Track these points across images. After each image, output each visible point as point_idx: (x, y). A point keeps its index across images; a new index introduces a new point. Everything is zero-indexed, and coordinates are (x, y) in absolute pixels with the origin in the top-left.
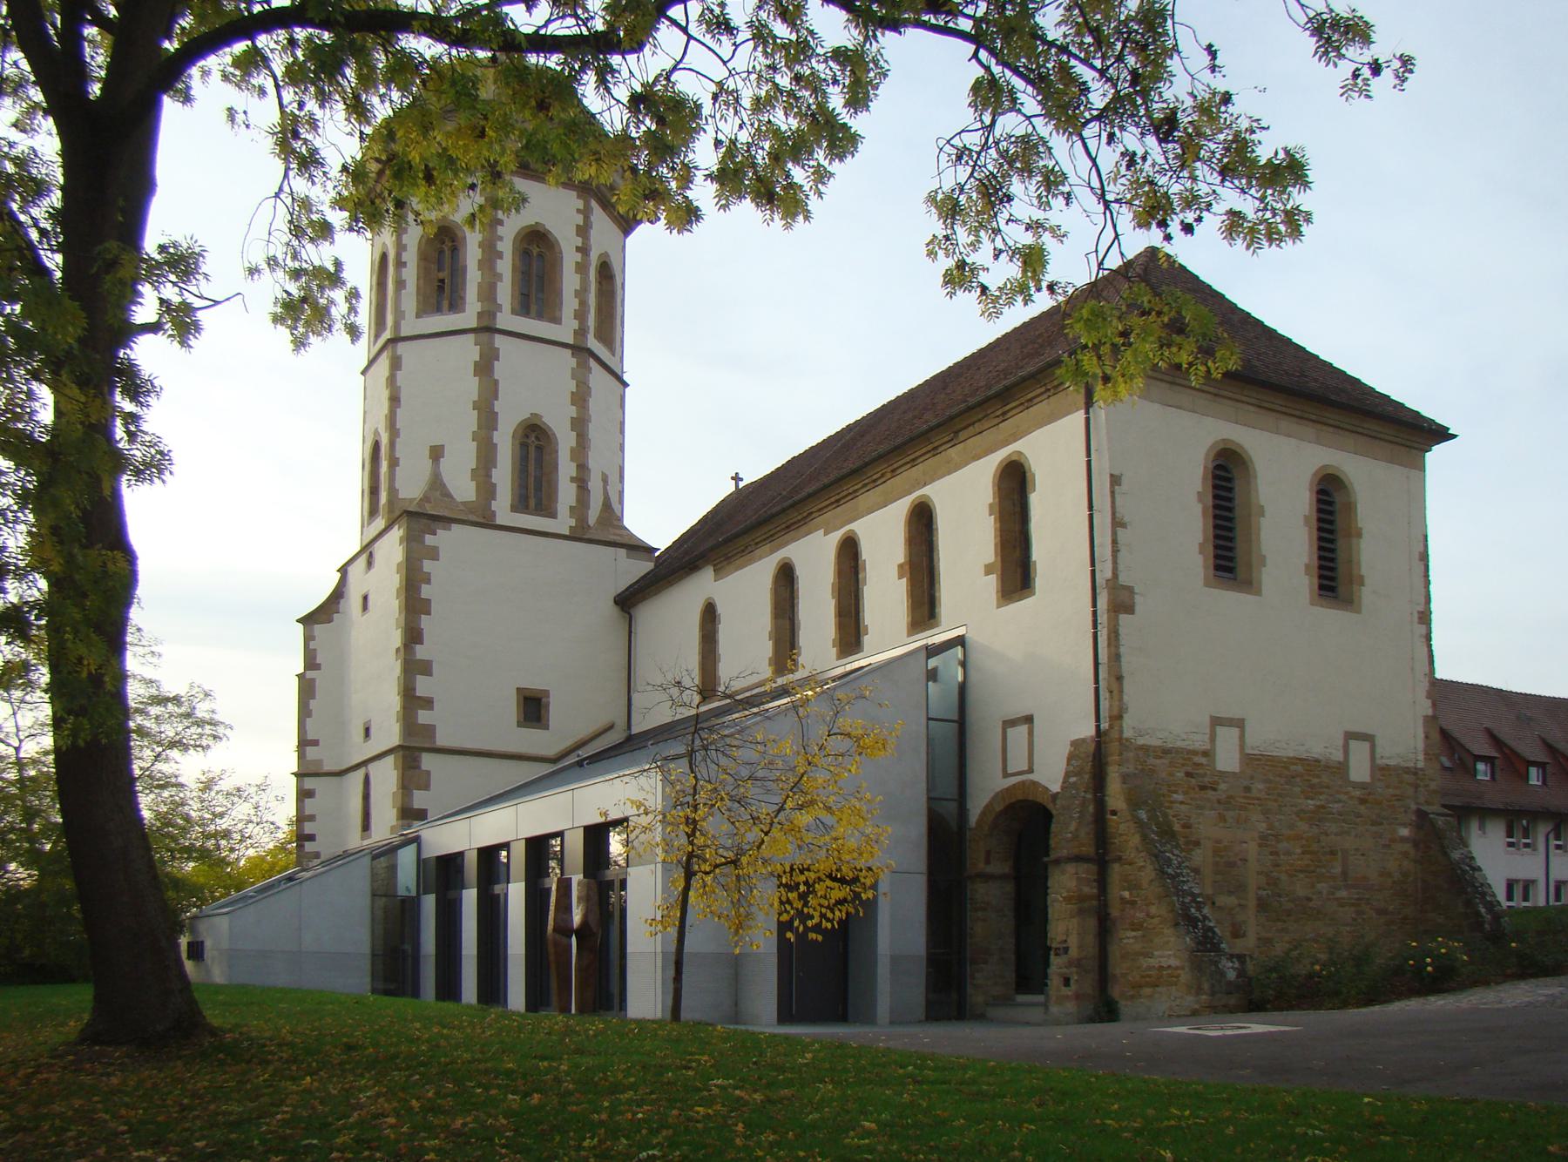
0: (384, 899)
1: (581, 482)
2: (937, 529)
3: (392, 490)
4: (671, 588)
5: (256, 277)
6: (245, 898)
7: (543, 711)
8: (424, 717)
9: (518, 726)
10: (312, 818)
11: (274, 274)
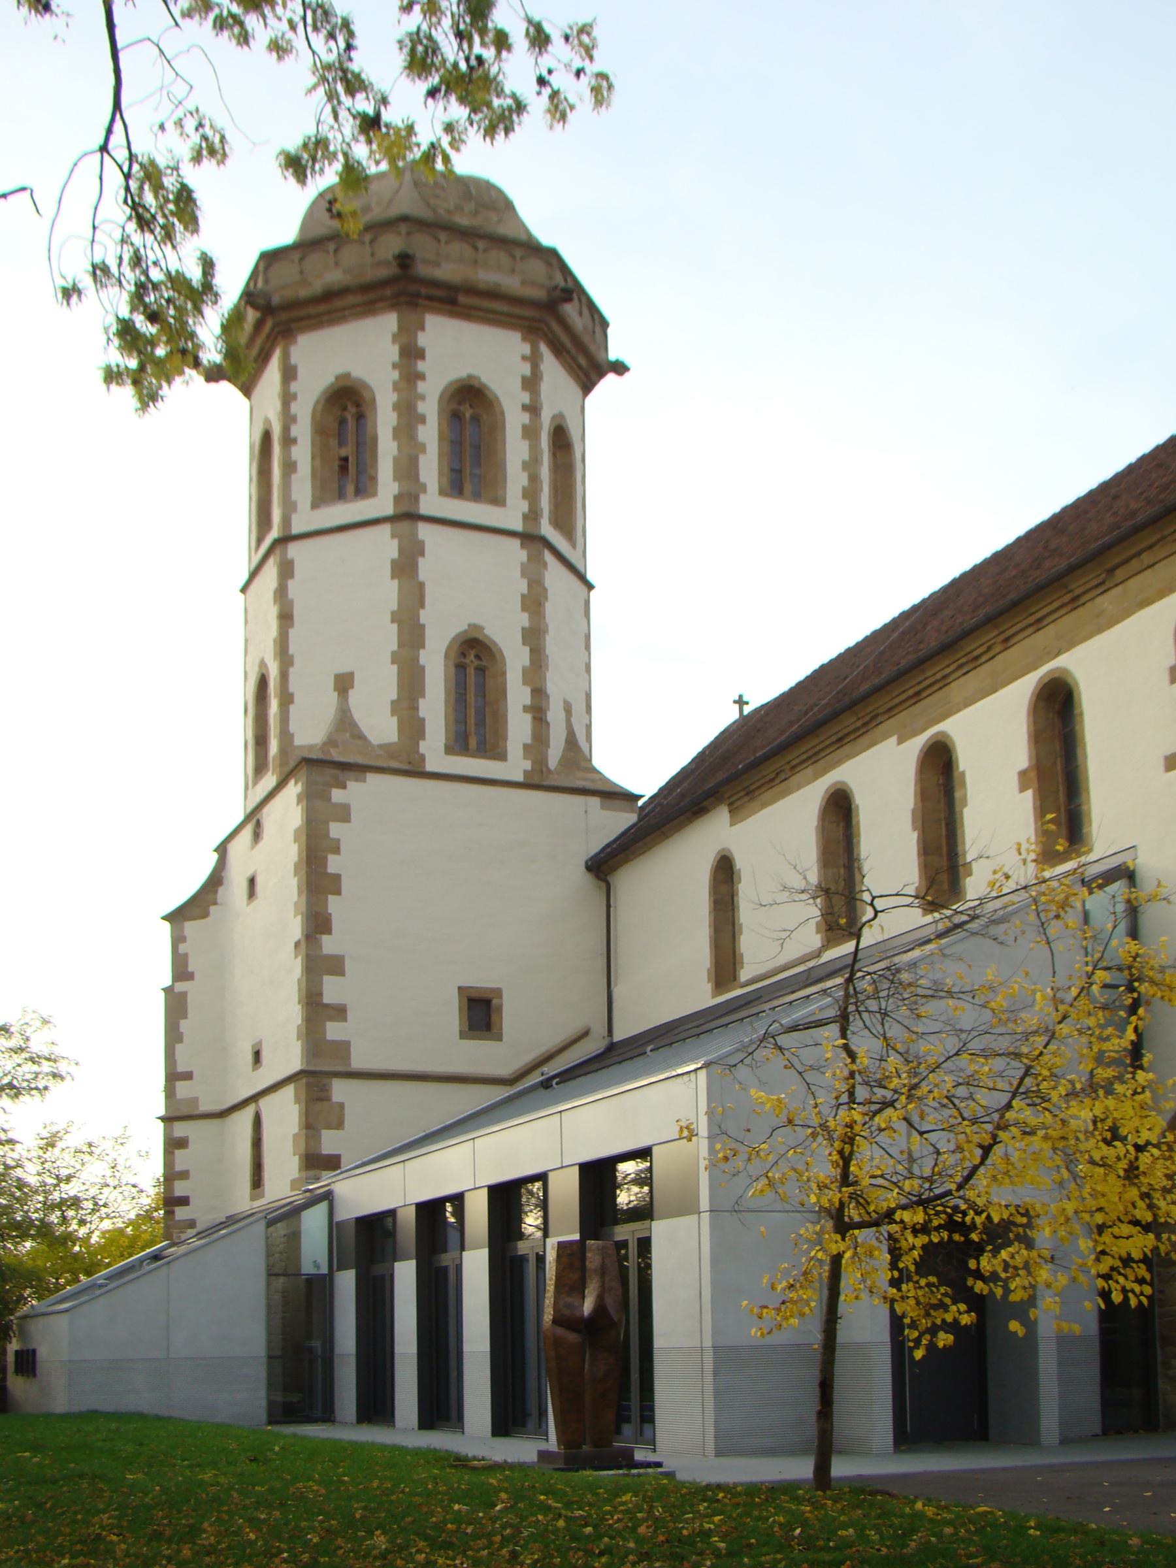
0: (282, 1280)
1: (538, 711)
2: (1081, 714)
3: (286, 736)
4: (666, 842)
5: (74, 299)
6: (94, 1286)
7: (494, 1017)
8: (334, 1031)
9: (461, 1038)
10: (184, 1175)
11: (103, 294)
